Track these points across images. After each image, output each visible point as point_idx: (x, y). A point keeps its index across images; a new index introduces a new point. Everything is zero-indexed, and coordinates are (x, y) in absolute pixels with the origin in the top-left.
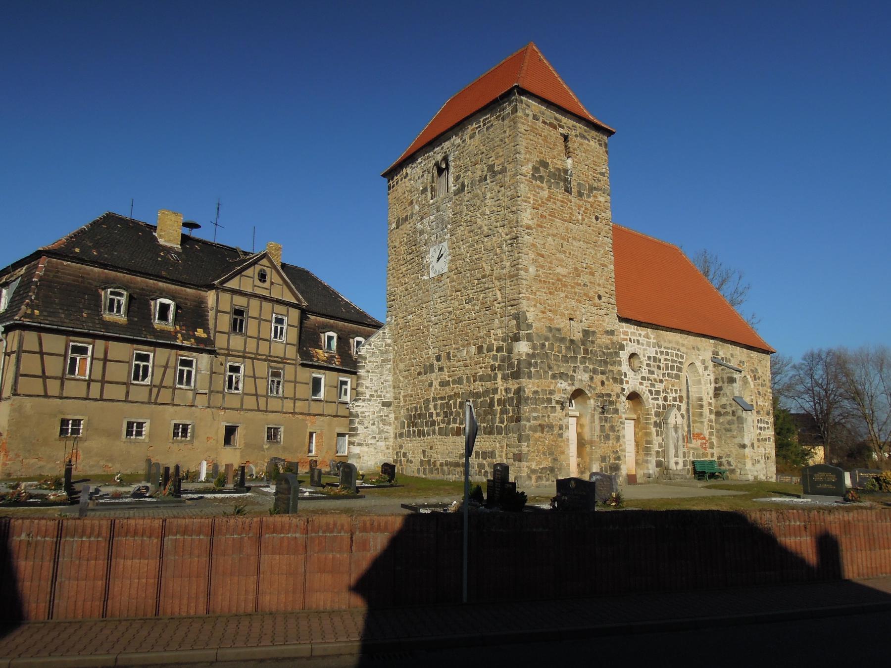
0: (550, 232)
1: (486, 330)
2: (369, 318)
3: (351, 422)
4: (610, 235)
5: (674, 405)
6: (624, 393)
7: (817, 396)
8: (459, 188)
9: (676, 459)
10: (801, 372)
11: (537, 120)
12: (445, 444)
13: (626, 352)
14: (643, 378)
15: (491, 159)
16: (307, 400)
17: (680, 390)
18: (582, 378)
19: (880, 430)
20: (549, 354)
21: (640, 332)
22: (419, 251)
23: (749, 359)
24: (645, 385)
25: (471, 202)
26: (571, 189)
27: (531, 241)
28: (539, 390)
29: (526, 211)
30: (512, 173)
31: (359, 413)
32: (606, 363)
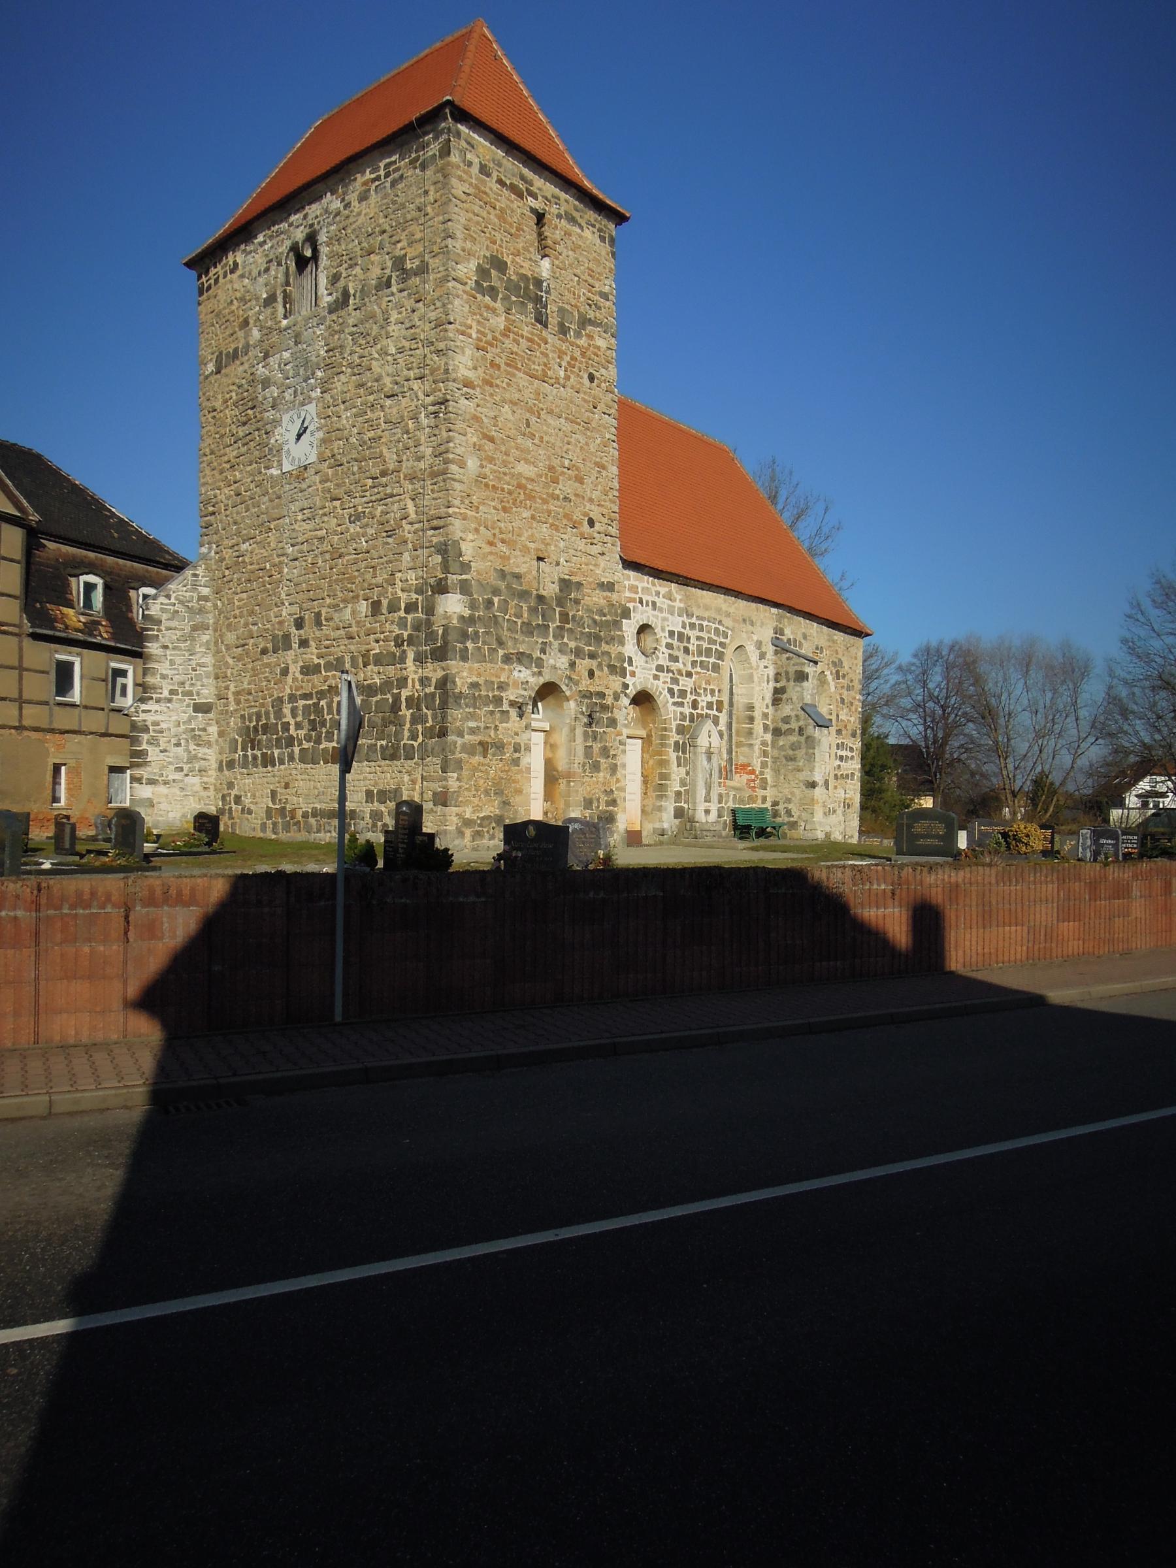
0: (507, 396)
1: (387, 573)
2: (168, 552)
3: (135, 741)
4: (613, 411)
5: (708, 716)
6: (627, 691)
7: (930, 716)
8: (338, 298)
9: (707, 804)
10: (910, 677)
11: (489, 175)
12: (313, 778)
13: (633, 621)
14: (660, 668)
15: (399, 245)
16: (47, 703)
17: (719, 691)
18: (557, 663)
19: (1016, 768)
20: (500, 619)
21: (658, 588)
22: (262, 418)
23: (830, 644)
24: (662, 680)
25: (361, 329)
26: (547, 318)
27: (473, 410)
28: (481, 682)
29: (463, 353)
31: (148, 723)
32: (598, 639)
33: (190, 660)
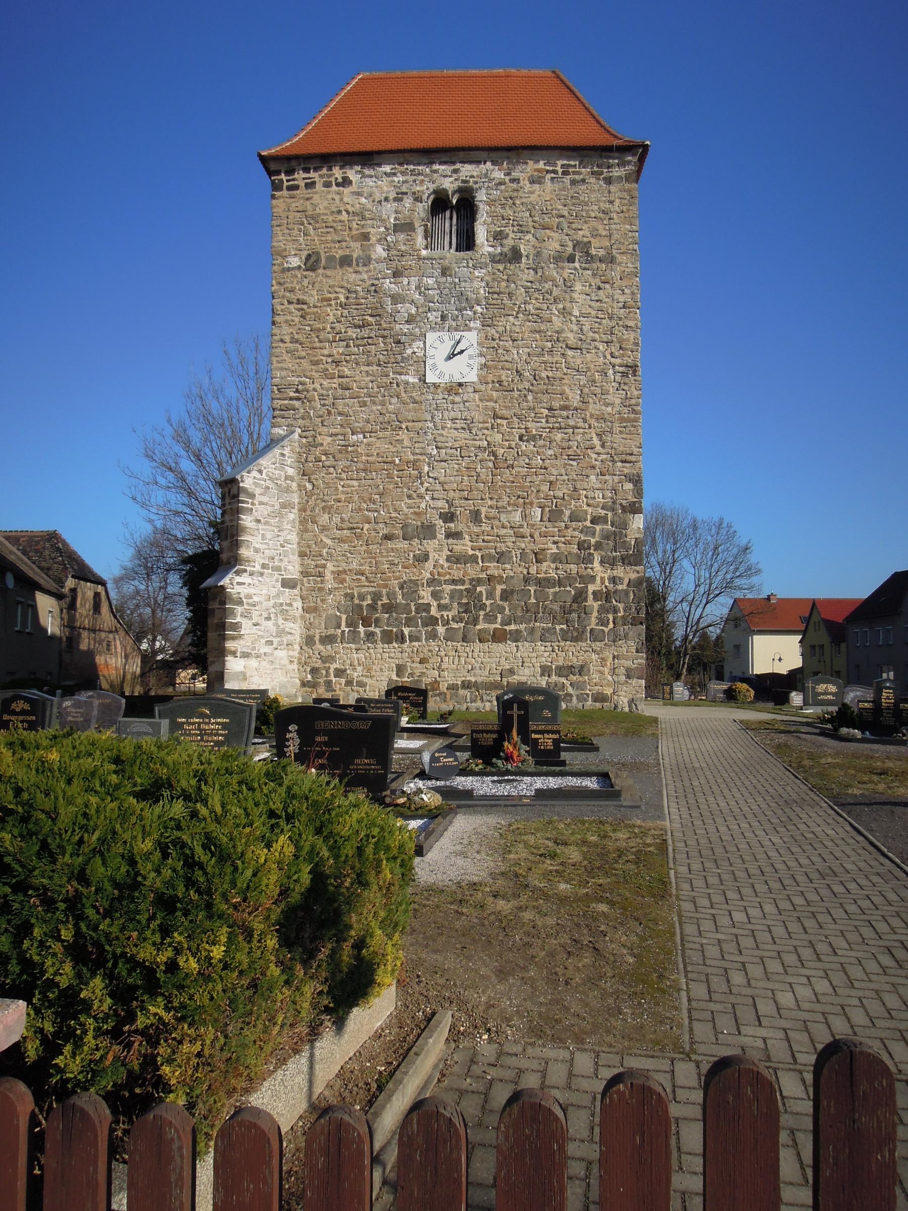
30: (627, 270)
31: (242, 596)
33: (278, 536)
